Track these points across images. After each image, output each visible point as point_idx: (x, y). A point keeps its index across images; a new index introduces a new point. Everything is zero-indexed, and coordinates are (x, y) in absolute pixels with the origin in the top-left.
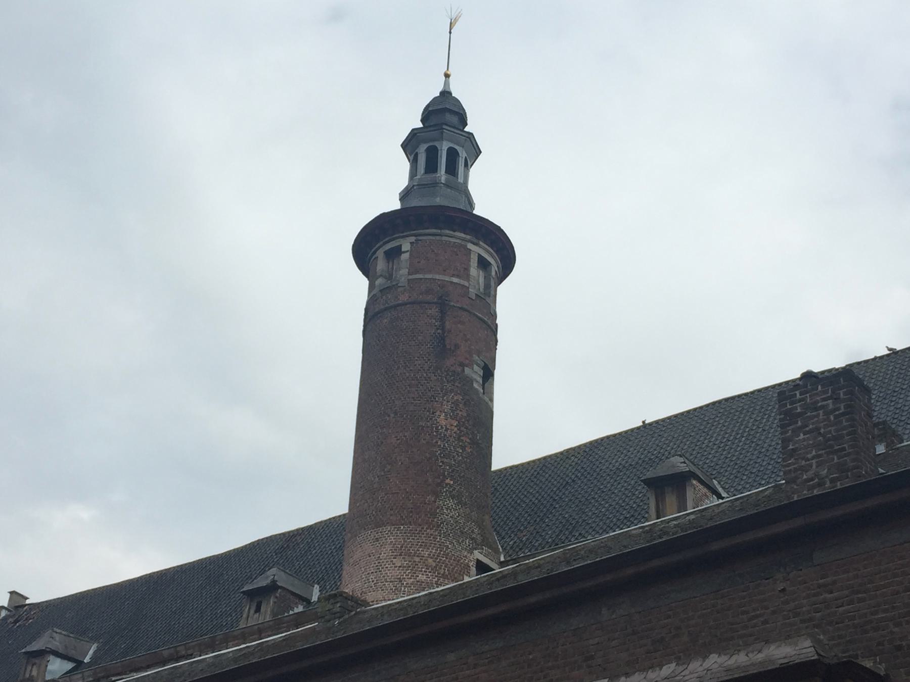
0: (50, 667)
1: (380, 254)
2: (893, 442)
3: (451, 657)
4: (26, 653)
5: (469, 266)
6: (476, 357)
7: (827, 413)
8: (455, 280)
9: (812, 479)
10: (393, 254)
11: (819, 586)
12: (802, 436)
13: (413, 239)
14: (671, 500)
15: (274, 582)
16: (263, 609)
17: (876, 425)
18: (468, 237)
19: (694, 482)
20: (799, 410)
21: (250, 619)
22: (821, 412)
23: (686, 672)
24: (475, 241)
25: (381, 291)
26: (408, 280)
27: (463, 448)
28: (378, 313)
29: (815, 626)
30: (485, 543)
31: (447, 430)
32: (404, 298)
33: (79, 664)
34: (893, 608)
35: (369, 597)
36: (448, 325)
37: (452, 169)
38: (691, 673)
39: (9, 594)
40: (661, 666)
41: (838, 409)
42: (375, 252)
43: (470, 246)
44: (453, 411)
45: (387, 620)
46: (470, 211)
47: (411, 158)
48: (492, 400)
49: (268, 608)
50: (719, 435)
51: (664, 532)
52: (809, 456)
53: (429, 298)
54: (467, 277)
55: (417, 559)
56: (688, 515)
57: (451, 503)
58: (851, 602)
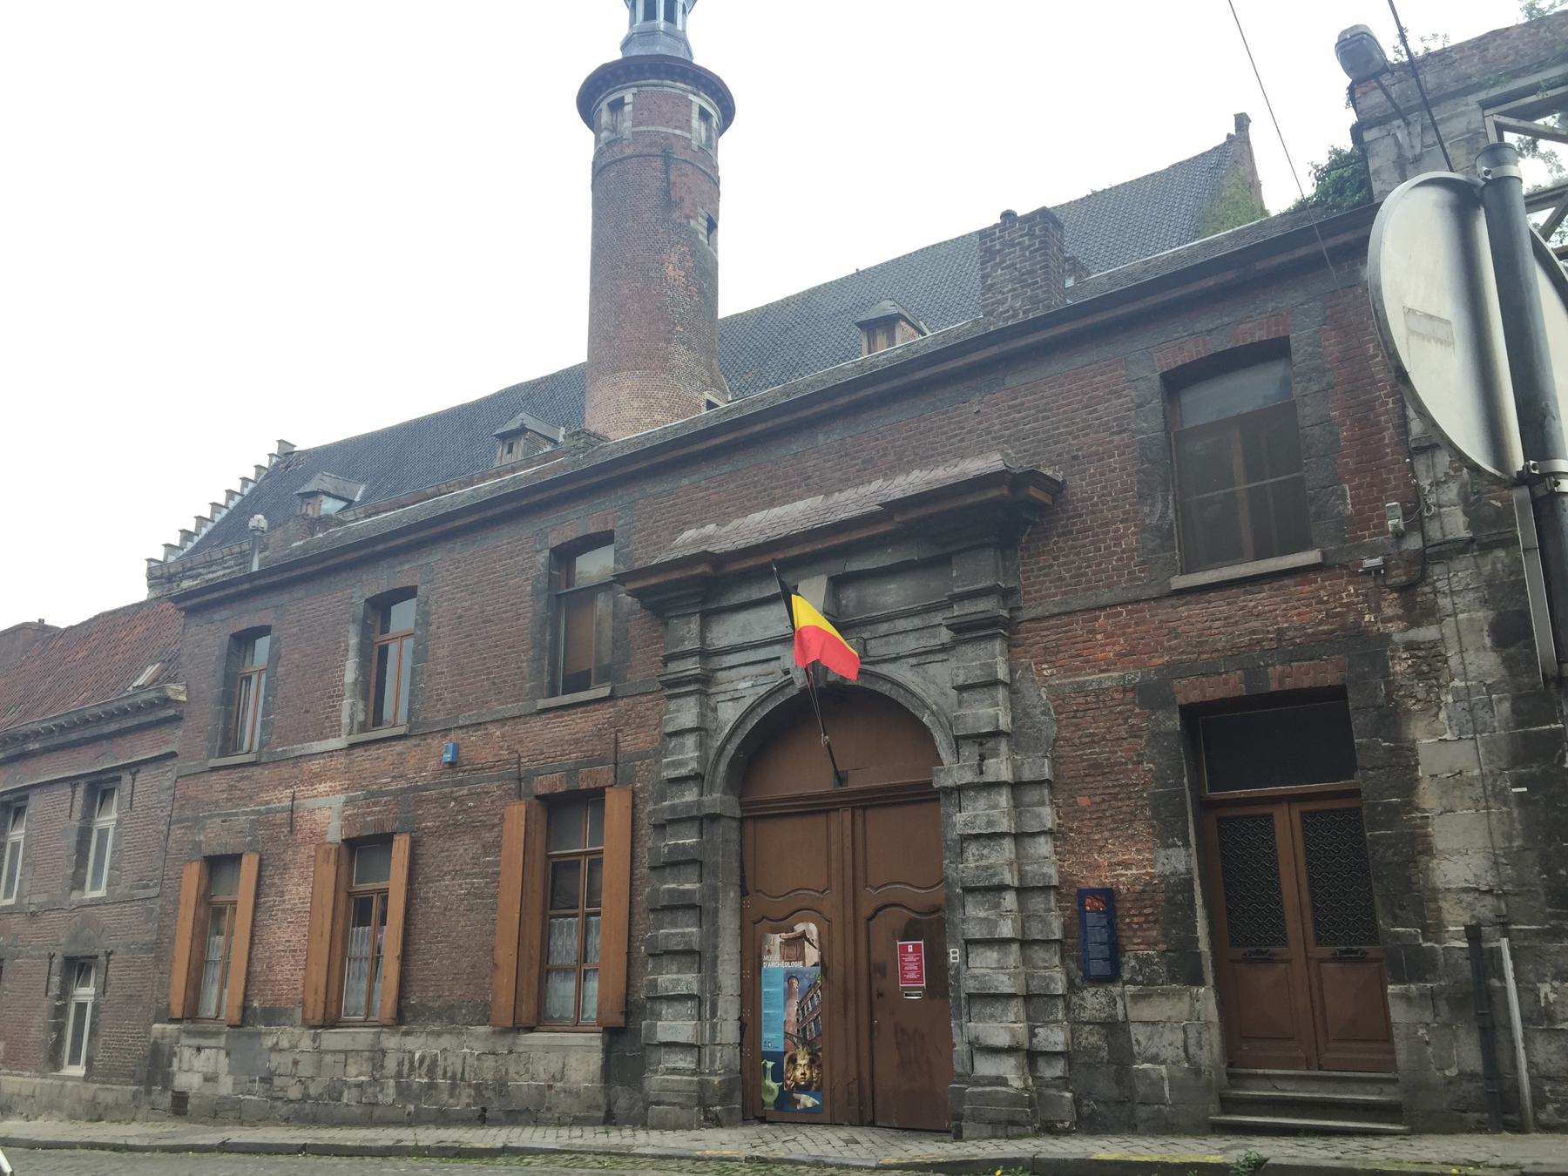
0: (324, 506)
1: (604, 106)
2: (1081, 276)
3: (685, 482)
4: (299, 494)
5: (691, 118)
6: (700, 210)
7: (1023, 249)
8: (678, 132)
9: (1007, 311)
10: (617, 106)
11: (1009, 407)
12: (999, 272)
13: (634, 90)
14: (881, 339)
15: (523, 425)
16: (514, 449)
17: (1067, 260)
18: (689, 88)
19: (903, 324)
20: (998, 247)
21: (503, 458)
22: (1018, 248)
23: (893, 486)
24: (695, 91)
25: (606, 144)
26: (633, 133)
27: (691, 297)
28: (604, 167)
29: (1004, 442)
30: (714, 384)
31: (675, 280)
32: (629, 151)
33: (350, 503)
34: (1073, 423)
35: (611, 435)
36: (672, 178)
37: (670, 16)
38: (896, 487)
39: (210, 507)
40: (870, 482)
41: (1034, 245)
42: (599, 104)
43: (691, 97)
44: (680, 262)
45: (627, 452)
46: (689, 59)
47: (630, 4)
48: (716, 251)
49: (520, 447)
50: (926, 279)
51: (873, 365)
52: (1006, 290)
53: (654, 150)
54: (690, 130)
55: (652, 401)
56: (896, 349)
57: (682, 348)
58: (1036, 420)
